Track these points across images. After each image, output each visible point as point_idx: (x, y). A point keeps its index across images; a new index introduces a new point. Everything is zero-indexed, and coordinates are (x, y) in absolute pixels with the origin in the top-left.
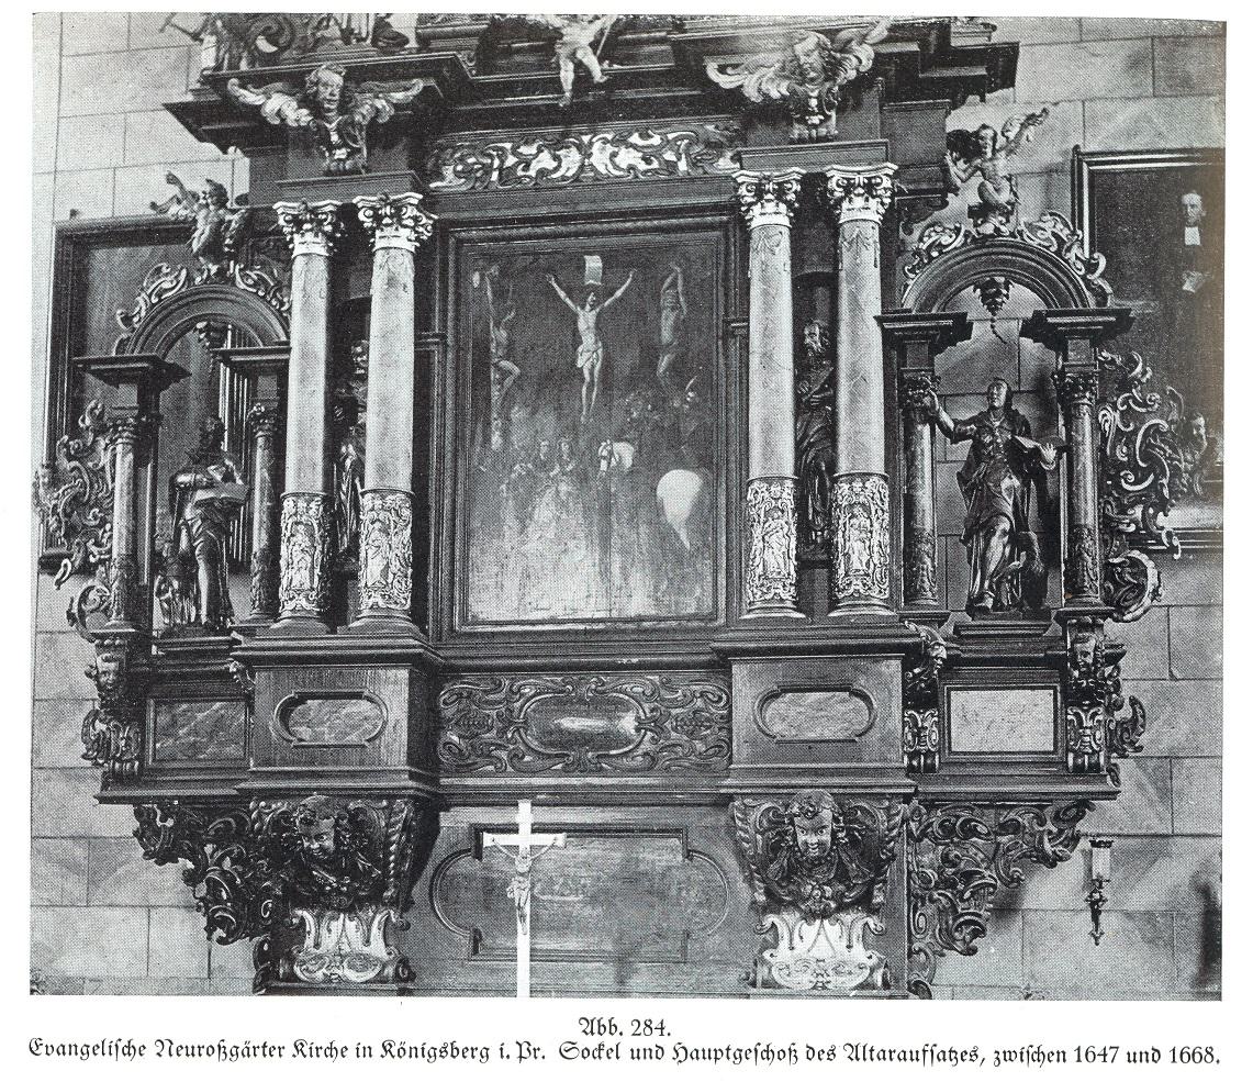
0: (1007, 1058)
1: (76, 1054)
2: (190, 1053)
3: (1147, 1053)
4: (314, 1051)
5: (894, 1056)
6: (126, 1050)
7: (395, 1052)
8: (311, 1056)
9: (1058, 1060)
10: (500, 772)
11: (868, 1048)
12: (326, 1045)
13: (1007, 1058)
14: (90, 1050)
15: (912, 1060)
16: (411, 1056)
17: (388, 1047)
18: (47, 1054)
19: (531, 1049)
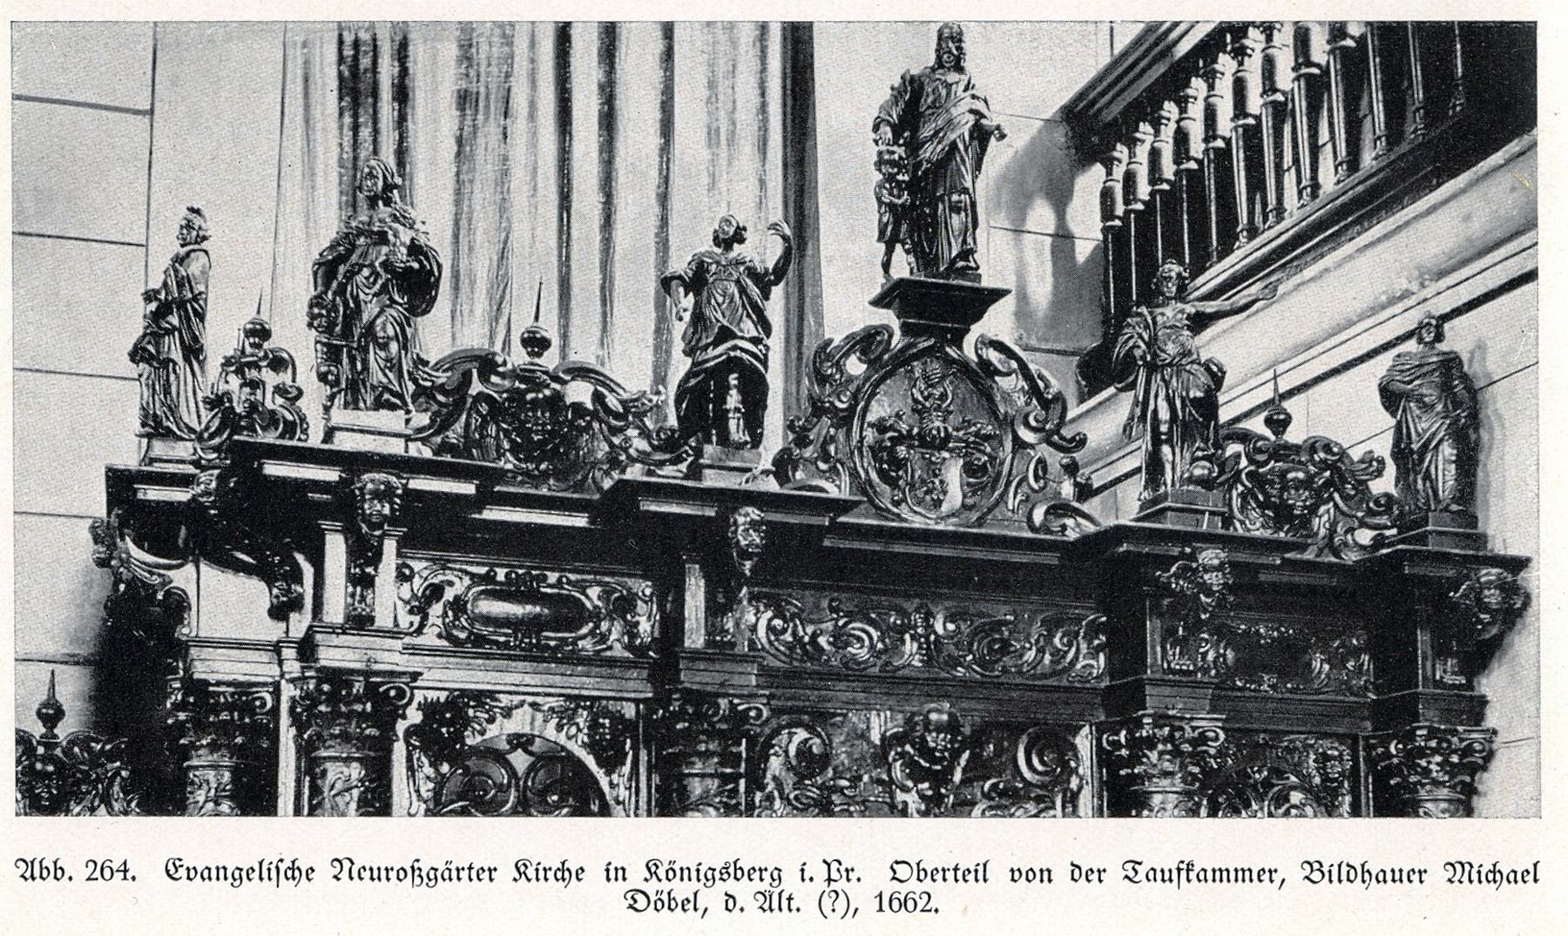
1: (226, 878)
2: (375, 876)
6: (290, 873)
7: (661, 873)
8: (538, 879)
11: (785, 896)
14: (244, 874)
18: (189, 878)
19: (842, 869)
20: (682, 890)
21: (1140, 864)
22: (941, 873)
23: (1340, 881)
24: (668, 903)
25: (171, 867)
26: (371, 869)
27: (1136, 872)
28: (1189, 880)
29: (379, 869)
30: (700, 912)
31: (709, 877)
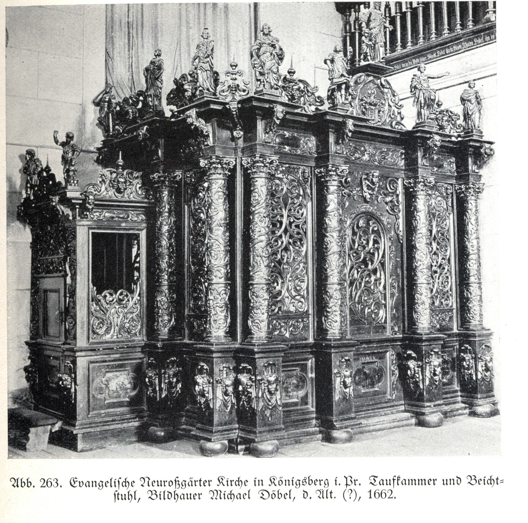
3: (453, 480)
4: (229, 483)
6: (124, 484)
8: (228, 485)
14: (104, 484)
15: (188, 499)
16: (190, 494)
19: (353, 480)
20: (284, 489)
21: (377, 477)
22: (208, 482)
23: (164, 499)
24: (279, 495)
25: (72, 482)
26: (158, 481)
27: (375, 481)
28: (398, 484)
29: (161, 481)
30: (292, 499)
31: (298, 483)
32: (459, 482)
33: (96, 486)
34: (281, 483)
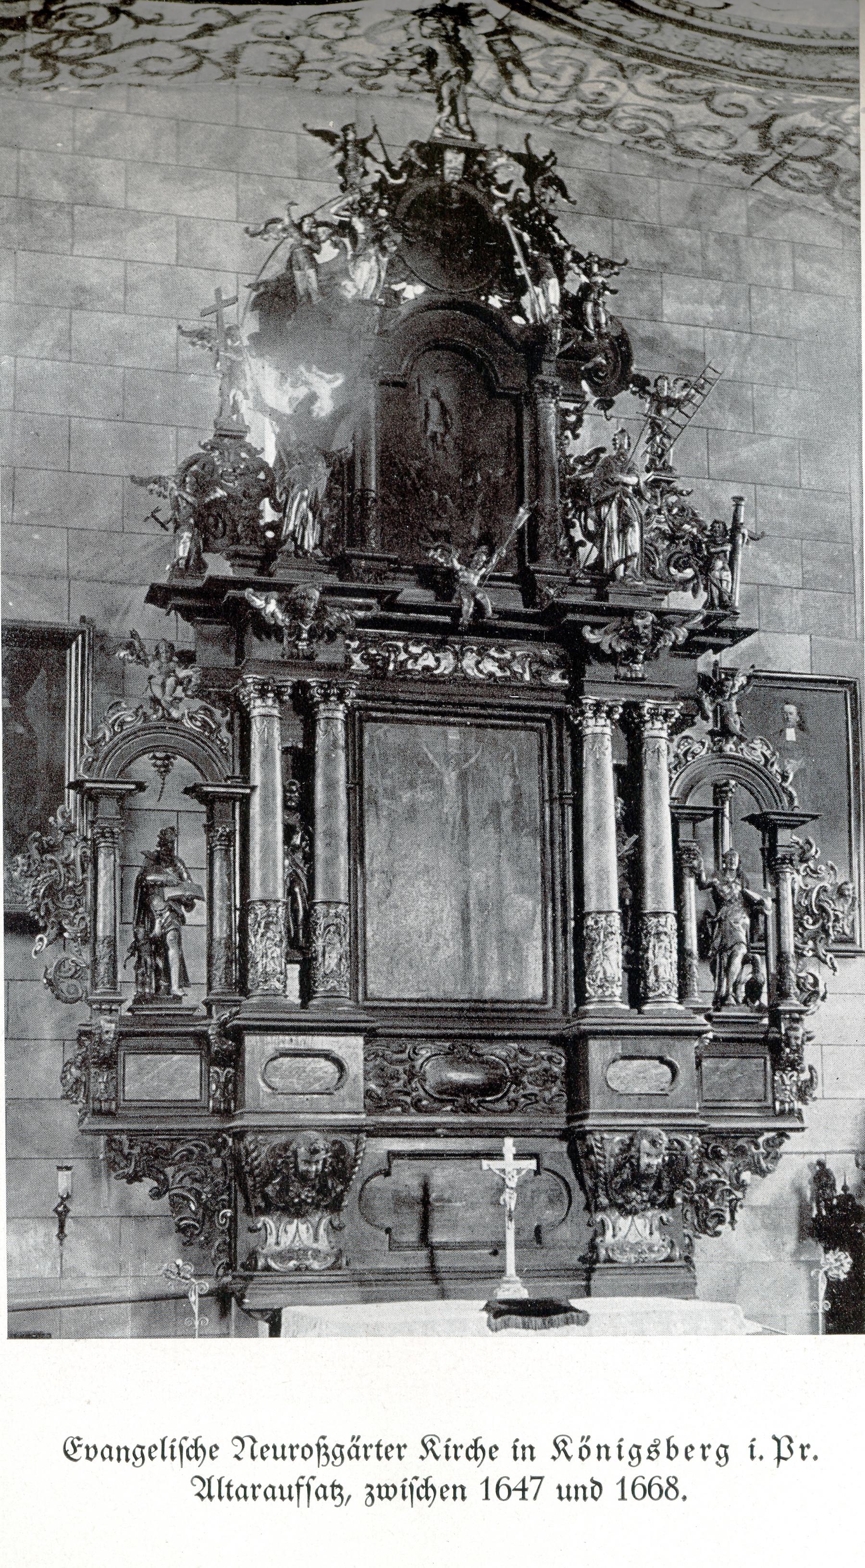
0: (384, 1494)
3: (584, 1488)
5: (259, 1492)
8: (447, 1457)
9: (455, 1498)
10: (405, 1111)
11: (224, 1483)
12: (469, 1442)
13: (384, 1494)
15: (282, 1498)
16: (599, 1458)
17: (429, 1445)
18: (88, 1458)
32: (596, 1494)
33: (127, 1460)
34: (585, 1452)
